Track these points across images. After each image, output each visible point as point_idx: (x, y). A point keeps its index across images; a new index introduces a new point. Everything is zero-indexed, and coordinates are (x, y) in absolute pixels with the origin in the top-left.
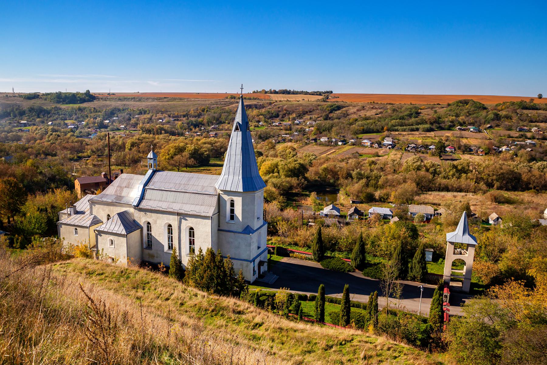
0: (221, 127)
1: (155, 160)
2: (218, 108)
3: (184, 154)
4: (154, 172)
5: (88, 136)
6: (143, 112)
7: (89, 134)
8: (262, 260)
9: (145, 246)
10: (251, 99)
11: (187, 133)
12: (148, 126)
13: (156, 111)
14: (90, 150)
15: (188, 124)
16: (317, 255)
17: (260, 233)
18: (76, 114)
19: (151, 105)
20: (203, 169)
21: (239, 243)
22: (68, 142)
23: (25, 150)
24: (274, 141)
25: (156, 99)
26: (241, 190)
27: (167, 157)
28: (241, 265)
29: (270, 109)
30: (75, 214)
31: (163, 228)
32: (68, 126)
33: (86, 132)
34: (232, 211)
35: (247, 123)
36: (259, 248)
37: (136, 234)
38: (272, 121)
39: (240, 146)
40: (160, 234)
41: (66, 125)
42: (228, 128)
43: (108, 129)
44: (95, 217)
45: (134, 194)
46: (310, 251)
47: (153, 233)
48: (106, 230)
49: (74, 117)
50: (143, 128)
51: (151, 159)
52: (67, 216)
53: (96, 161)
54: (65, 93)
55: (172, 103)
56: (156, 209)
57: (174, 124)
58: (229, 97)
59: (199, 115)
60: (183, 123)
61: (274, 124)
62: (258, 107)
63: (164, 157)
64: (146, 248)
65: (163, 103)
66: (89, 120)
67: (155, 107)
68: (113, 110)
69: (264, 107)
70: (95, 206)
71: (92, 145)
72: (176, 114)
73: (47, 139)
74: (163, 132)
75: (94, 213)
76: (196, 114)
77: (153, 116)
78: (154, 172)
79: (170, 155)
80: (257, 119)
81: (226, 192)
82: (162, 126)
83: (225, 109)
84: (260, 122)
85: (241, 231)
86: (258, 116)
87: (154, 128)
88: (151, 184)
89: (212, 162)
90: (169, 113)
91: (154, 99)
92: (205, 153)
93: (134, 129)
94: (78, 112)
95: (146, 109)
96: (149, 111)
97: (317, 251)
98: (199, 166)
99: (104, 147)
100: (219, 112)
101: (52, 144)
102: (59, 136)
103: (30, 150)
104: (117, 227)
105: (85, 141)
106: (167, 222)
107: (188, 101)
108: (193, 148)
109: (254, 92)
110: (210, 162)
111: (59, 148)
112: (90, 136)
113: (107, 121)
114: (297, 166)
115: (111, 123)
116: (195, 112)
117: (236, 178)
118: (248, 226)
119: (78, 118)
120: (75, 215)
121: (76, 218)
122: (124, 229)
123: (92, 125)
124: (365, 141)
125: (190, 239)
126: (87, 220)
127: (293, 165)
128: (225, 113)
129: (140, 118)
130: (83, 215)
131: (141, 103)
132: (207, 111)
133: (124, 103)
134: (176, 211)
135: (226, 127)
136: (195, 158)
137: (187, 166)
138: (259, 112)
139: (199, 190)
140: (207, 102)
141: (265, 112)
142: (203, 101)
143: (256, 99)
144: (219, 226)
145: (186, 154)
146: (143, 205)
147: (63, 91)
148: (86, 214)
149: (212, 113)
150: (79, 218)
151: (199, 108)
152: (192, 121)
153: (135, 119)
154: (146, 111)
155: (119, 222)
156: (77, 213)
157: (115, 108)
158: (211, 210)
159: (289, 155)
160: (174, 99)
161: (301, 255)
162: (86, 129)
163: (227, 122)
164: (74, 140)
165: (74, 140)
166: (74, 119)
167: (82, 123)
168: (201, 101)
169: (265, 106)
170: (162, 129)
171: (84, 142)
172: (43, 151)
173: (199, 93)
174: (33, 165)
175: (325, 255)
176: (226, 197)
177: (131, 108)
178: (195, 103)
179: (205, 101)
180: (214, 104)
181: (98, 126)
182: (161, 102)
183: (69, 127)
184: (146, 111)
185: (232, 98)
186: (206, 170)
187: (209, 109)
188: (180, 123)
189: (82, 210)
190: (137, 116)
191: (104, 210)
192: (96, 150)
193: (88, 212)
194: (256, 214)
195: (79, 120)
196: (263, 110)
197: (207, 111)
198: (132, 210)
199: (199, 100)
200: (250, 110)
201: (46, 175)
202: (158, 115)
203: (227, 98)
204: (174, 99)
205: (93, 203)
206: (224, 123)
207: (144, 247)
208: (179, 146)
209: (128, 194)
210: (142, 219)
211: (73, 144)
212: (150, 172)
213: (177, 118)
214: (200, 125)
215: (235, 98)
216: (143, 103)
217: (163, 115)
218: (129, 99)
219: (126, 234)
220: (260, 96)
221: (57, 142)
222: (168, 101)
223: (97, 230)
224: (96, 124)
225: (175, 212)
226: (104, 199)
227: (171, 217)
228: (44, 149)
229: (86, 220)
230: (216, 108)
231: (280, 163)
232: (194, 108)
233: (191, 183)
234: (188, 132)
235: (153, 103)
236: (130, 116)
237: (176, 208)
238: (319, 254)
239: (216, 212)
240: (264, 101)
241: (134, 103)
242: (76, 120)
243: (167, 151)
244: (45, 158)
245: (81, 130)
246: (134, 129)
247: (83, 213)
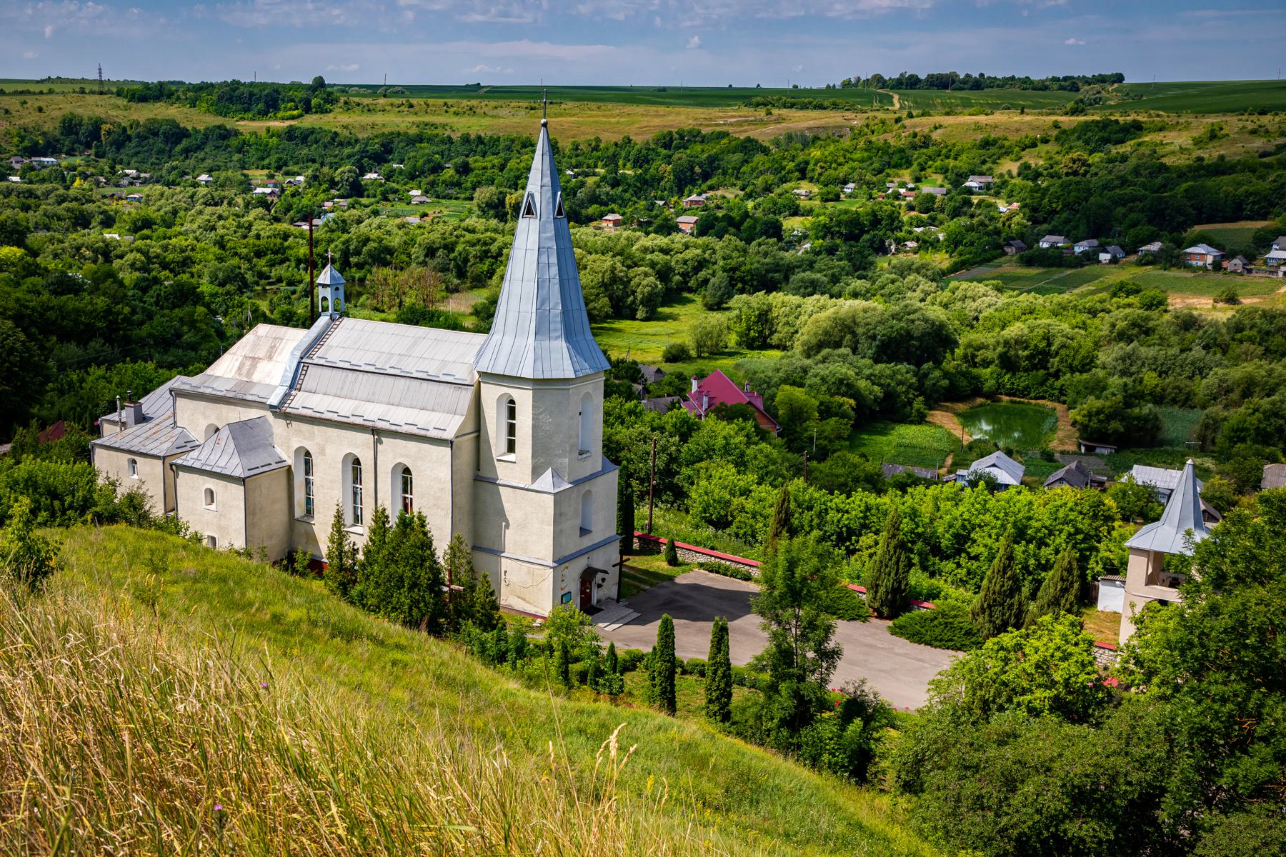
17: (589, 492)
36: (584, 531)
48: (198, 465)
52: (118, 429)
54: (252, 84)
121: (138, 433)
124: (1200, 249)
125: (405, 498)
126: (163, 439)
139: (433, 370)
147: (246, 79)
158: (451, 424)
237: (373, 413)
239: (470, 427)
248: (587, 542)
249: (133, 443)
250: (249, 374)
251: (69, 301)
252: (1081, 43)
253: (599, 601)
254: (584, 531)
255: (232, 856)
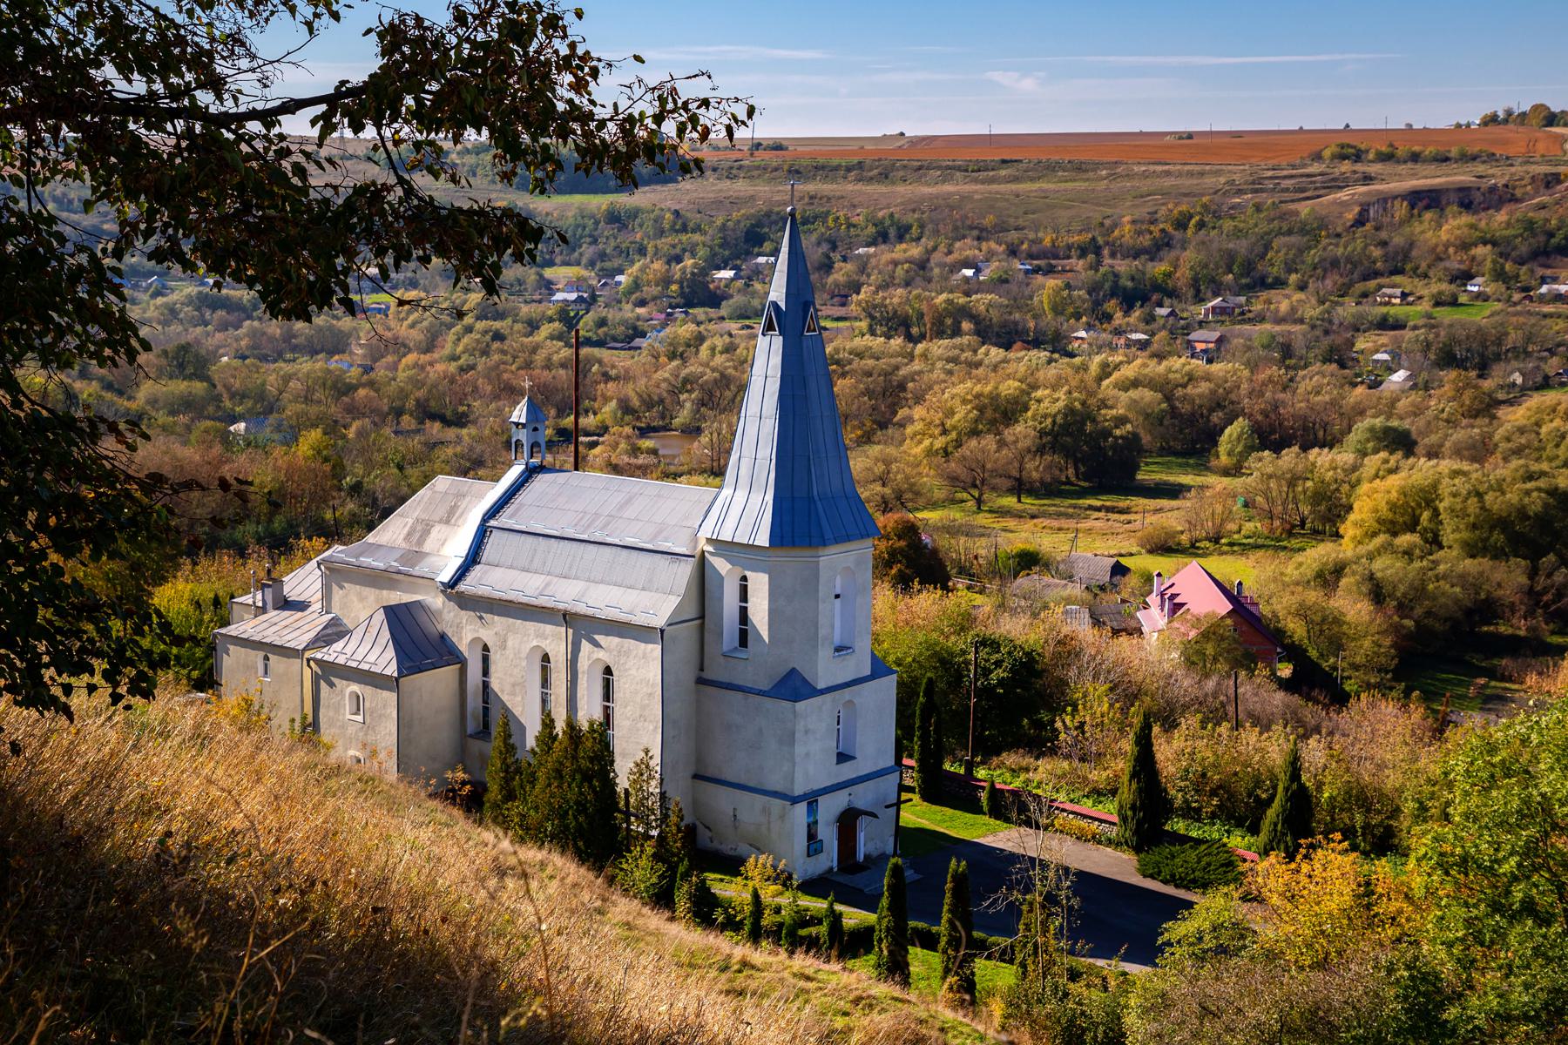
0: (1257, 307)
1: (535, 429)
2: (1258, 208)
3: (1009, 434)
4: (531, 473)
5: (632, 338)
6: (892, 232)
7: (635, 332)
8: (860, 804)
9: (471, 727)
10: (1447, 159)
11: (1082, 334)
12: (896, 296)
13: (956, 229)
14: (614, 404)
15: (1093, 289)
16: (1132, 825)
18: (595, 241)
19: (931, 197)
20: (1098, 503)
21: (760, 730)
22: (528, 365)
23: (345, 394)
24: (1518, 378)
25: (959, 169)
26: (763, 539)
27: (939, 443)
28: (766, 811)
29: (1543, 207)
30: (276, 609)
31: (524, 663)
32: (552, 293)
33: (624, 322)
34: (744, 612)
35: (807, 304)
36: (843, 758)
37: (436, 683)
38: (1540, 272)
39: (774, 386)
40: (514, 685)
41: (548, 286)
42: (1293, 310)
43: (723, 312)
44: (335, 622)
45: (451, 549)
46: (1109, 809)
47: (495, 684)
49: (588, 251)
50: (875, 307)
51: (524, 426)
53: (627, 452)
55: (1036, 186)
56: (505, 597)
57: (1027, 292)
58: (1327, 153)
59: (1154, 251)
60: (1068, 286)
61: (1544, 289)
62: (1478, 197)
63: (927, 442)
64: (473, 736)
65: (995, 187)
66: (643, 270)
67: (952, 208)
68: (759, 224)
69: (1514, 200)
70: (342, 587)
71: (626, 377)
72: (1047, 242)
73: (447, 350)
74: (966, 325)
75: (336, 611)
76: (1146, 241)
77: (935, 248)
78: (531, 473)
79: (954, 435)
80: (1455, 263)
81: (723, 547)
82: (962, 300)
83: (1297, 213)
84: (1471, 277)
85: (765, 685)
86: (1465, 246)
87: (924, 307)
88: (509, 510)
89: (1148, 474)
90: (1013, 236)
91: (949, 171)
92: (1118, 432)
93: (841, 311)
94: (606, 230)
95: (910, 218)
96: (922, 226)
97: (1133, 807)
98: (1083, 494)
99: (675, 392)
100: (1264, 227)
101: (462, 370)
102: (498, 336)
103: (362, 392)
104: (377, 650)
105: (600, 362)
106: (535, 643)
107: (1113, 177)
108: (1060, 404)
109: (1491, 120)
110: (1139, 477)
111: (489, 388)
112: (637, 342)
113: (727, 274)
114: (1536, 503)
115: (740, 283)
116: (1139, 233)
117: (756, 499)
118: (793, 670)
119: (603, 256)
120: (277, 612)
122: (394, 661)
123: (655, 290)
126: (306, 628)
127: (1512, 497)
128: (1290, 232)
129: (873, 261)
130: (300, 614)
131: (890, 189)
132: (1201, 225)
133: (811, 187)
134: (561, 606)
135: (1284, 306)
136: (1068, 453)
137: (1020, 487)
138: (1472, 227)
140: (1209, 181)
141: (1508, 224)
142: (1191, 174)
143: (1474, 158)
144: (702, 669)
145: (1023, 431)
146: (474, 584)
148: (310, 610)
149: (1220, 239)
150: (284, 623)
151: (1163, 211)
152: (1116, 275)
153: (849, 267)
154: (908, 228)
155: (386, 634)
156: (285, 604)
157: (768, 214)
159: (1550, 451)
160: (1050, 168)
161: (1084, 823)
162: (628, 307)
163: (1293, 278)
164: (555, 358)
165: (555, 358)
166: (584, 261)
167: (619, 278)
168: (1180, 175)
169: (1518, 193)
170: (965, 312)
171: (595, 369)
172: (417, 401)
173: (1190, 136)
174: (319, 452)
175: (1167, 828)
176: (721, 565)
177: (841, 214)
178: (1145, 186)
179: (1202, 174)
180: (1240, 192)
181: (682, 294)
182: (983, 182)
183: (559, 296)
184: (908, 228)
185: (1344, 157)
186: (1098, 509)
187: (1213, 214)
188: (1052, 283)
189: (301, 598)
190: (861, 251)
191: (362, 599)
192: (643, 401)
193: (317, 606)
194: (822, 632)
195: (608, 265)
196: (1501, 217)
197: (1201, 225)
198: (436, 601)
199: (1168, 173)
200: (1428, 215)
201: (375, 500)
202: (958, 245)
203: (1318, 157)
204: (1050, 168)
205: (335, 575)
206: (1279, 283)
207: (469, 731)
208: (994, 397)
209: (443, 544)
210: (465, 631)
211: (546, 376)
212: (516, 471)
213: (1046, 260)
214: (1155, 297)
215: (1358, 156)
216: (901, 189)
217: (984, 246)
218: (837, 168)
219: (396, 674)
220: (1506, 142)
221: (482, 363)
222: (1016, 180)
223: (315, 660)
224: (674, 287)
225: (559, 610)
226: (367, 561)
227: (548, 628)
228: (421, 394)
229: (296, 631)
230: (1250, 211)
231: (1445, 488)
232: (1142, 212)
233: (630, 512)
234: (1089, 327)
235: (948, 188)
236: (834, 248)
237: (567, 594)
238: (1140, 824)
239: (691, 611)
240: (1518, 169)
241: (859, 187)
242: (591, 264)
243: (938, 417)
244: (418, 431)
245: (604, 313)
246: (841, 311)
247: (301, 606)
248: (848, 771)
249: (265, 633)
250: (421, 542)
251: (719, 876)
252: (96, 120)
253: (867, 857)
254: (843, 758)
255: (4, 494)
